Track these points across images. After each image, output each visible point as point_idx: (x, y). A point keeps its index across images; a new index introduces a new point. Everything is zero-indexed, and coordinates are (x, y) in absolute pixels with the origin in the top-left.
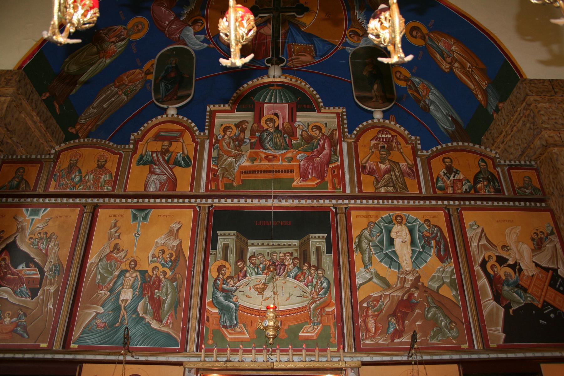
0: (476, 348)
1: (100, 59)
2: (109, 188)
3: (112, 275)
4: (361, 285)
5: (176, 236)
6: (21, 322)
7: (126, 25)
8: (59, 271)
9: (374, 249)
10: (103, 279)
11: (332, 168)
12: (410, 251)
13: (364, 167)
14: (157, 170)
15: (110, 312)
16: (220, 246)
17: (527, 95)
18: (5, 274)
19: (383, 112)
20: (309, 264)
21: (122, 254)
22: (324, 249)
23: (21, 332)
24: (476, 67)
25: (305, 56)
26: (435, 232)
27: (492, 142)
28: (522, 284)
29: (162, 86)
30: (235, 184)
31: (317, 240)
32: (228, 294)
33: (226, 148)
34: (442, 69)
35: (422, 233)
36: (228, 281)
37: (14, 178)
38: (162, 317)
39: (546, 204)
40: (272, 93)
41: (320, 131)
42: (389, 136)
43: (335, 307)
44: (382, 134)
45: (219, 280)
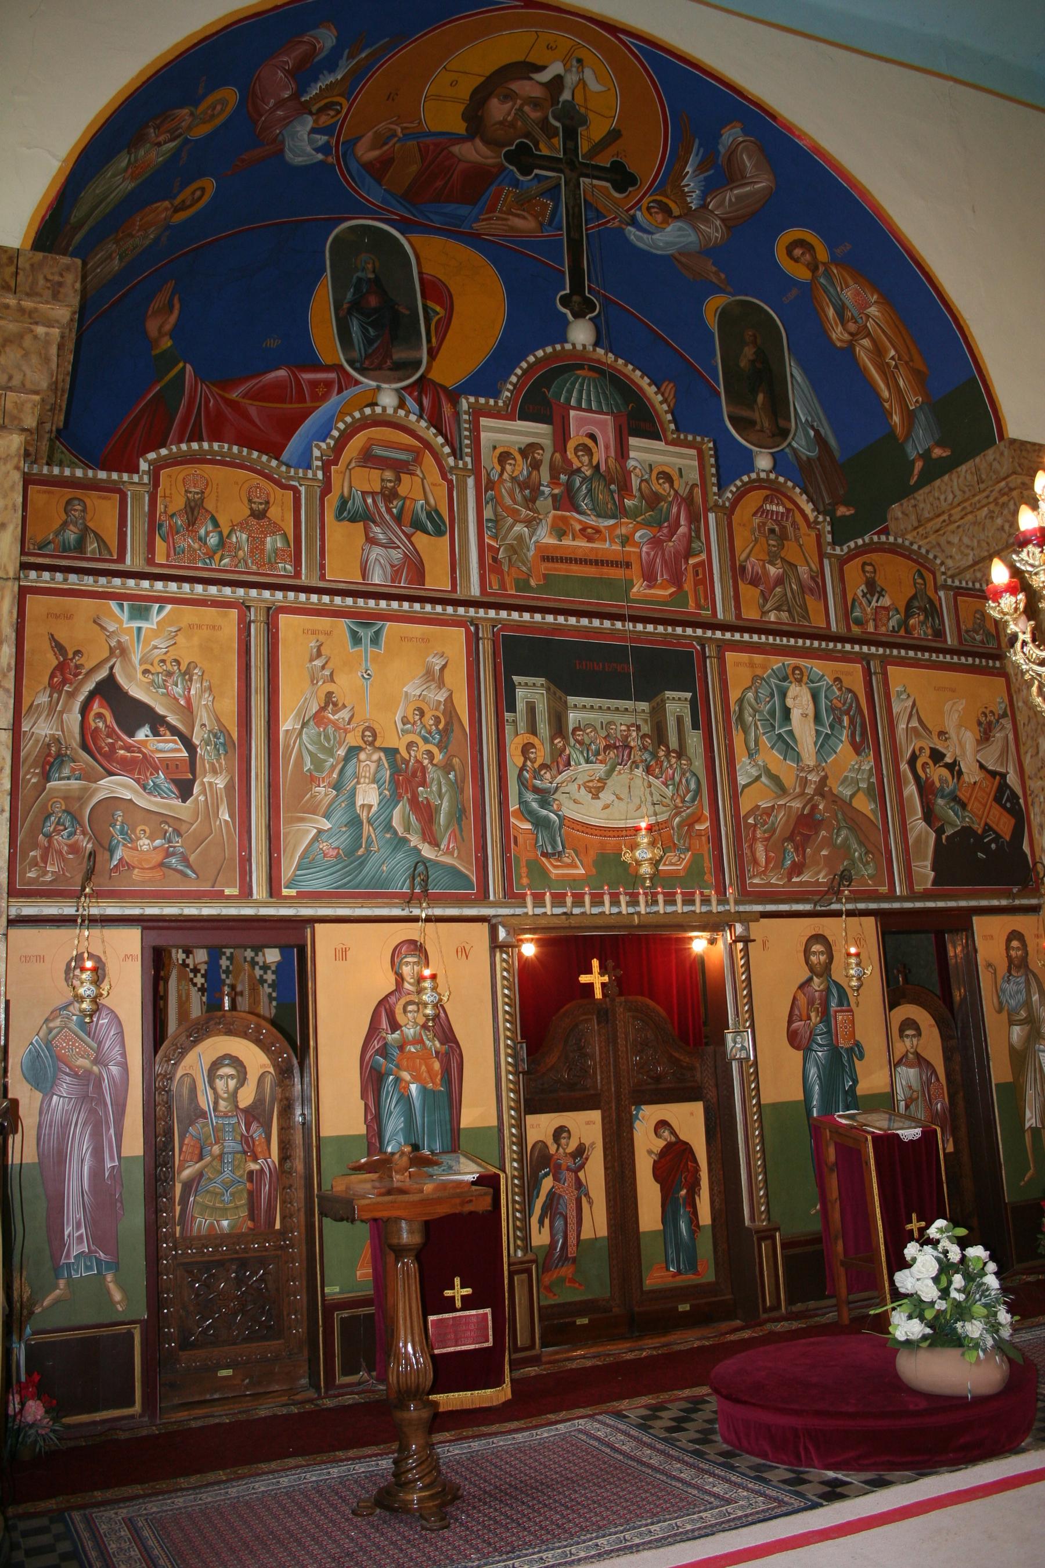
0: (898, 893)
2: (288, 567)
3: (332, 755)
4: (745, 786)
5: (441, 684)
6: (174, 847)
8: (224, 745)
9: (762, 725)
10: (318, 764)
11: (695, 566)
12: (813, 732)
13: (743, 568)
14: (381, 536)
15: (344, 829)
16: (520, 706)
17: (1014, 473)
18: (112, 746)
19: (772, 454)
20: (667, 747)
21: (344, 714)
22: (688, 721)
23: (180, 867)
24: (907, 363)
25: (524, 218)
26: (849, 701)
27: (916, 524)
28: (962, 797)
30: (533, 583)
31: (676, 704)
32: (545, 797)
33: (508, 501)
34: (830, 339)
35: (831, 701)
36: (542, 772)
37: (65, 524)
38: (438, 836)
39: (1001, 664)
41: (672, 486)
42: (781, 509)
43: (708, 824)
44: (771, 503)
45: (527, 771)
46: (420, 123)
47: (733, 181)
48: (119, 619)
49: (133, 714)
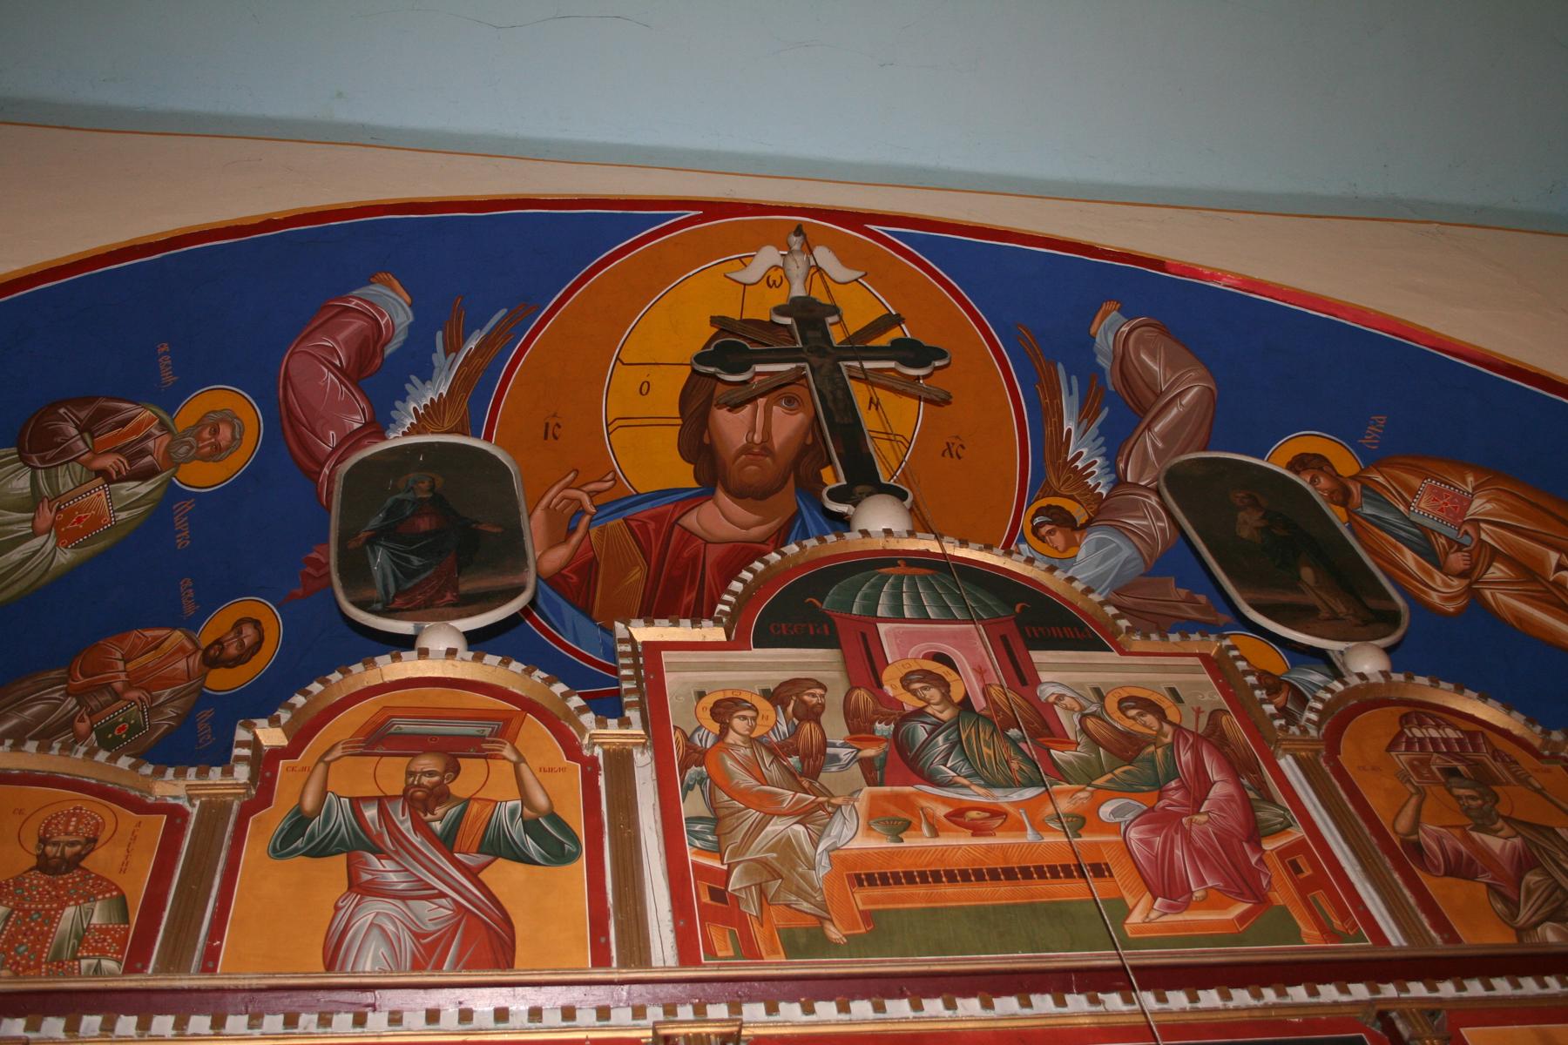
1: (34, 535)
7: (170, 412)
11: (1282, 853)
13: (1416, 849)
14: (393, 877)
19: (1388, 650)
29: (380, 560)
30: (834, 933)
40: (897, 589)
42: (1451, 733)
46: (615, 479)
47: (1146, 412)
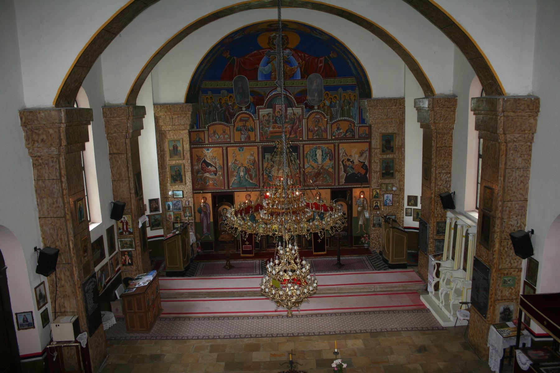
48: (205, 151)
49: (208, 165)
